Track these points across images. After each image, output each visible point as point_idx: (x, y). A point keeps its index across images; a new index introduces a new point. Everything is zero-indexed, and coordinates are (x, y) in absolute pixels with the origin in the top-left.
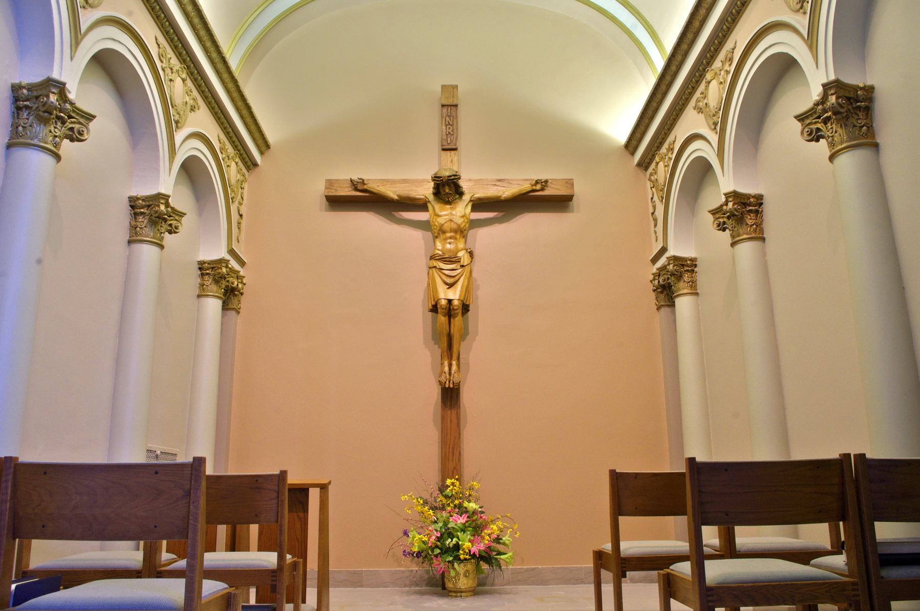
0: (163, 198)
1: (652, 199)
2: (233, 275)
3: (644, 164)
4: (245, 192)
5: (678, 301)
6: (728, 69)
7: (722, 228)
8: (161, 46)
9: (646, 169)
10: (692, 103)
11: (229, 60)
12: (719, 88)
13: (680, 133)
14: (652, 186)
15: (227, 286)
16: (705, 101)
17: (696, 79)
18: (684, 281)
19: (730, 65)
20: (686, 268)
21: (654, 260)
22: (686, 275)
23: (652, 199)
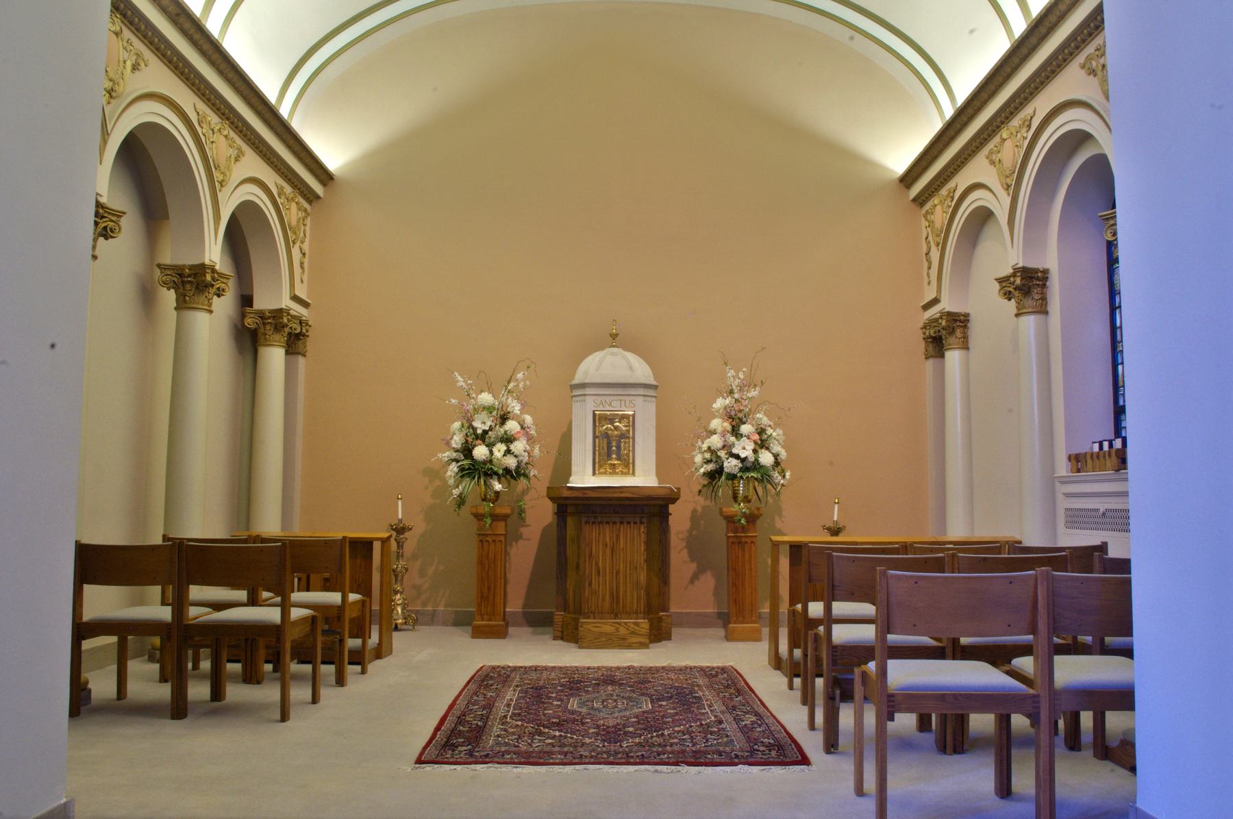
0: (209, 268)
1: (926, 238)
2: (295, 321)
3: (921, 200)
4: (308, 228)
5: (948, 354)
6: (1025, 135)
7: (1008, 295)
8: (200, 113)
9: (922, 205)
10: (1081, 58)
11: (292, 125)
12: (1014, 151)
13: (962, 181)
14: (927, 225)
15: (290, 334)
16: (1102, 61)
17: (1083, 37)
18: (956, 337)
19: (1027, 132)
20: (958, 324)
21: (926, 307)
22: (959, 331)
23: (926, 238)
